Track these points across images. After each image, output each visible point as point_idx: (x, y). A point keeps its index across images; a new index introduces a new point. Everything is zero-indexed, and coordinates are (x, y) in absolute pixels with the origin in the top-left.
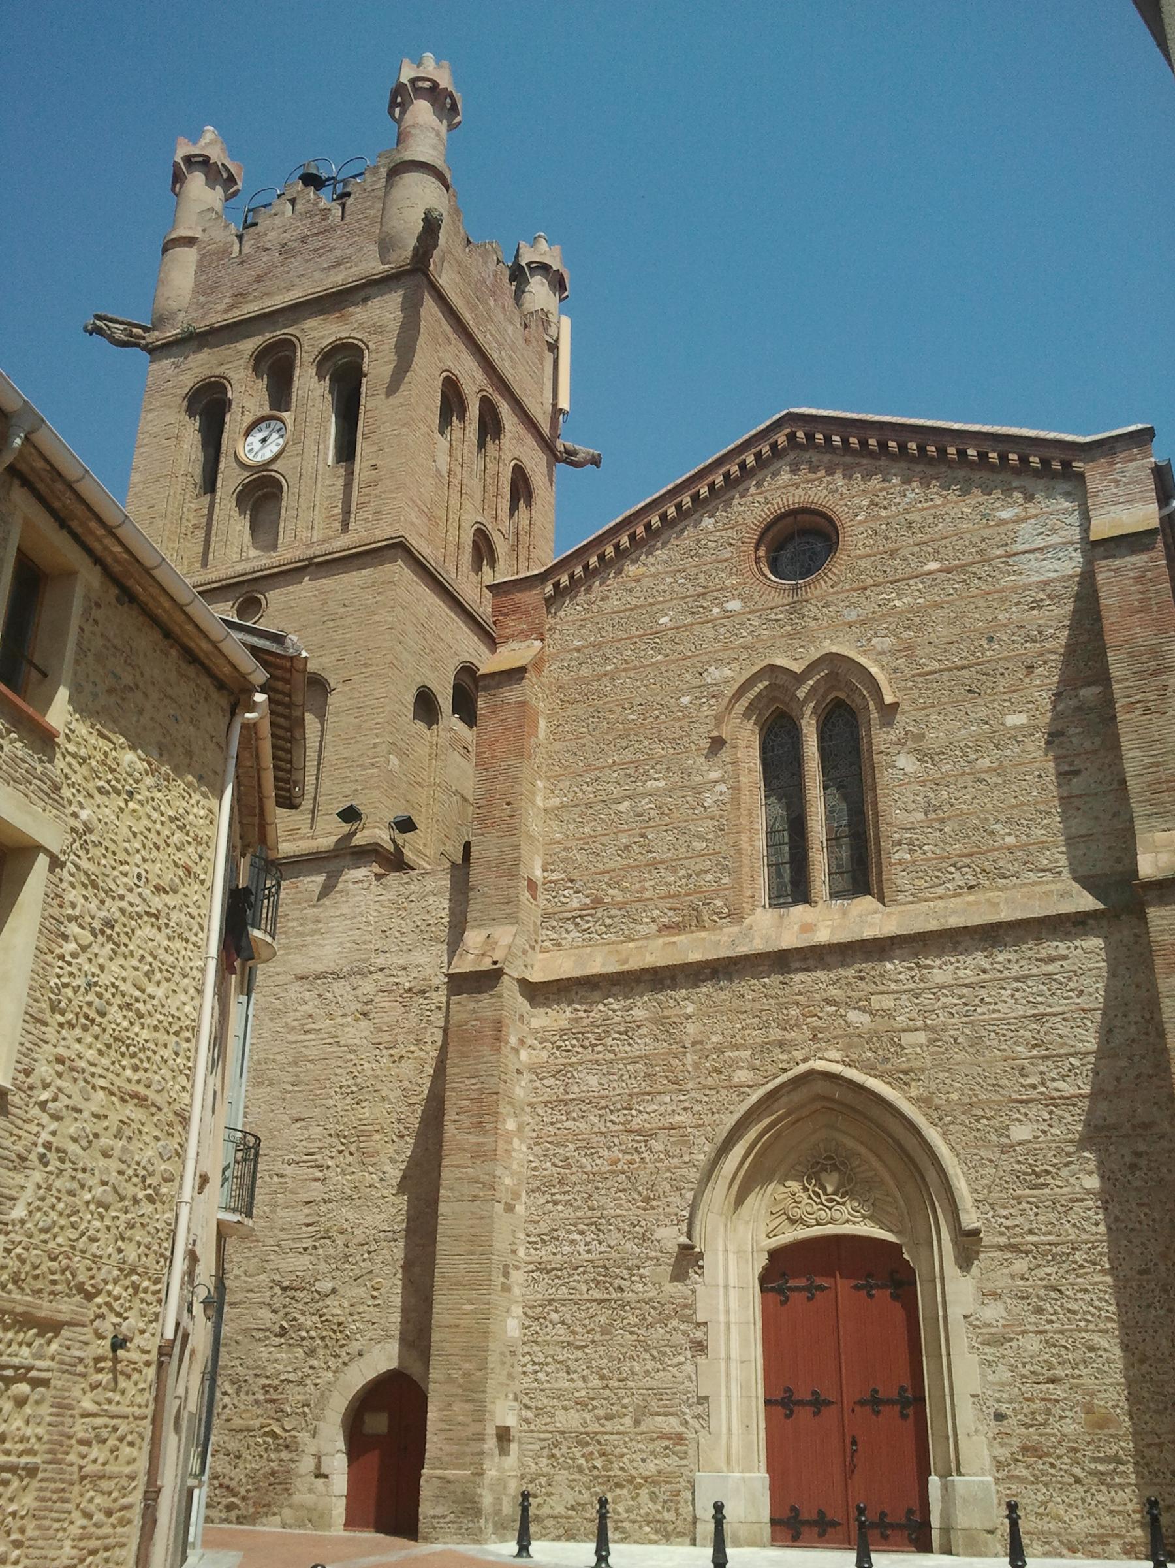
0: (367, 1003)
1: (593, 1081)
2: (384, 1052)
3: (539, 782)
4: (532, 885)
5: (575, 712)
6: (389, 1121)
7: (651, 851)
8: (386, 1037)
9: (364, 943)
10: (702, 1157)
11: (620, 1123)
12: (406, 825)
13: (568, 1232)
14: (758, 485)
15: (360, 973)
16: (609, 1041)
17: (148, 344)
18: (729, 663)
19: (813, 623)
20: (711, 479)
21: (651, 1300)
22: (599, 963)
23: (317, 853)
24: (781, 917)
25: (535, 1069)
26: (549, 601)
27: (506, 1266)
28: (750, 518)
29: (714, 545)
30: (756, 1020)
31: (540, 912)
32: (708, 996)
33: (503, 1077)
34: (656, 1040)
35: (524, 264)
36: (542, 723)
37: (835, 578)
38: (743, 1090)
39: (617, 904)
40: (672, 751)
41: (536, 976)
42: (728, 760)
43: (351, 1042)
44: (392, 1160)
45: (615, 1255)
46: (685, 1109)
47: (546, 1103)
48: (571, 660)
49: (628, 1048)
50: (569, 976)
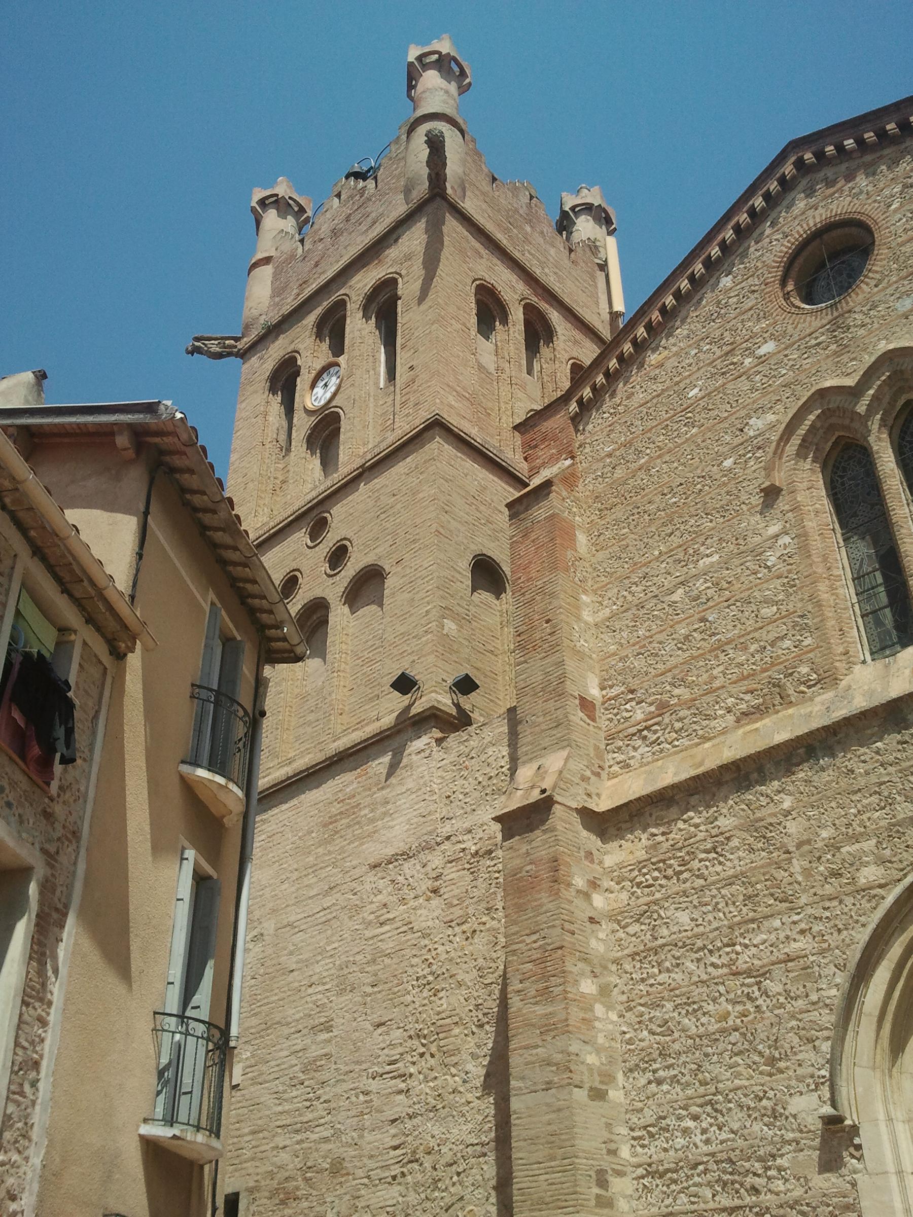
0: (437, 878)
1: (684, 918)
2: (458, 930)
3: (584, 597)
4: (586, 705)
5: (614, 517)
6: (467, 1009)
7: (714, 634)
8: (457, 912)
9: (429, 814)
10: (834, 992)
11: (723, 965)
12: (466, 685)
13: (680, 1118)
14: (773, 225)
15: (428, 847)
16: (695, 864)
17: (239, 350)
18: (771, 408)
19: (862, 332)
20: (720, 238)
21: (796, 1202)
22: (672, 772)
23: (381, 732)
24: (887, 666)
25: (615, 917)
26: (576, 420)
27: (601, 1173)
28: (769, 258)
29: (735, 300)
30: (875, 799)
31: (603, 735)
32: (808, 782)
33: (567, 926)
34: (752, 850)
35: (567, 209)
36: (582, 538)
37: (878, 276)
38: (873, 892)
39: (685, 703)
40: (722, 520)
41: (602, 805)
42: (787, 507)
43: (424, 925)
44: (474, 1056)
45: (740, 1142)
46: (802, 932)
47: (633, 956)
48: (604, 467)
49: (719, 868)
50: (637, 796)
